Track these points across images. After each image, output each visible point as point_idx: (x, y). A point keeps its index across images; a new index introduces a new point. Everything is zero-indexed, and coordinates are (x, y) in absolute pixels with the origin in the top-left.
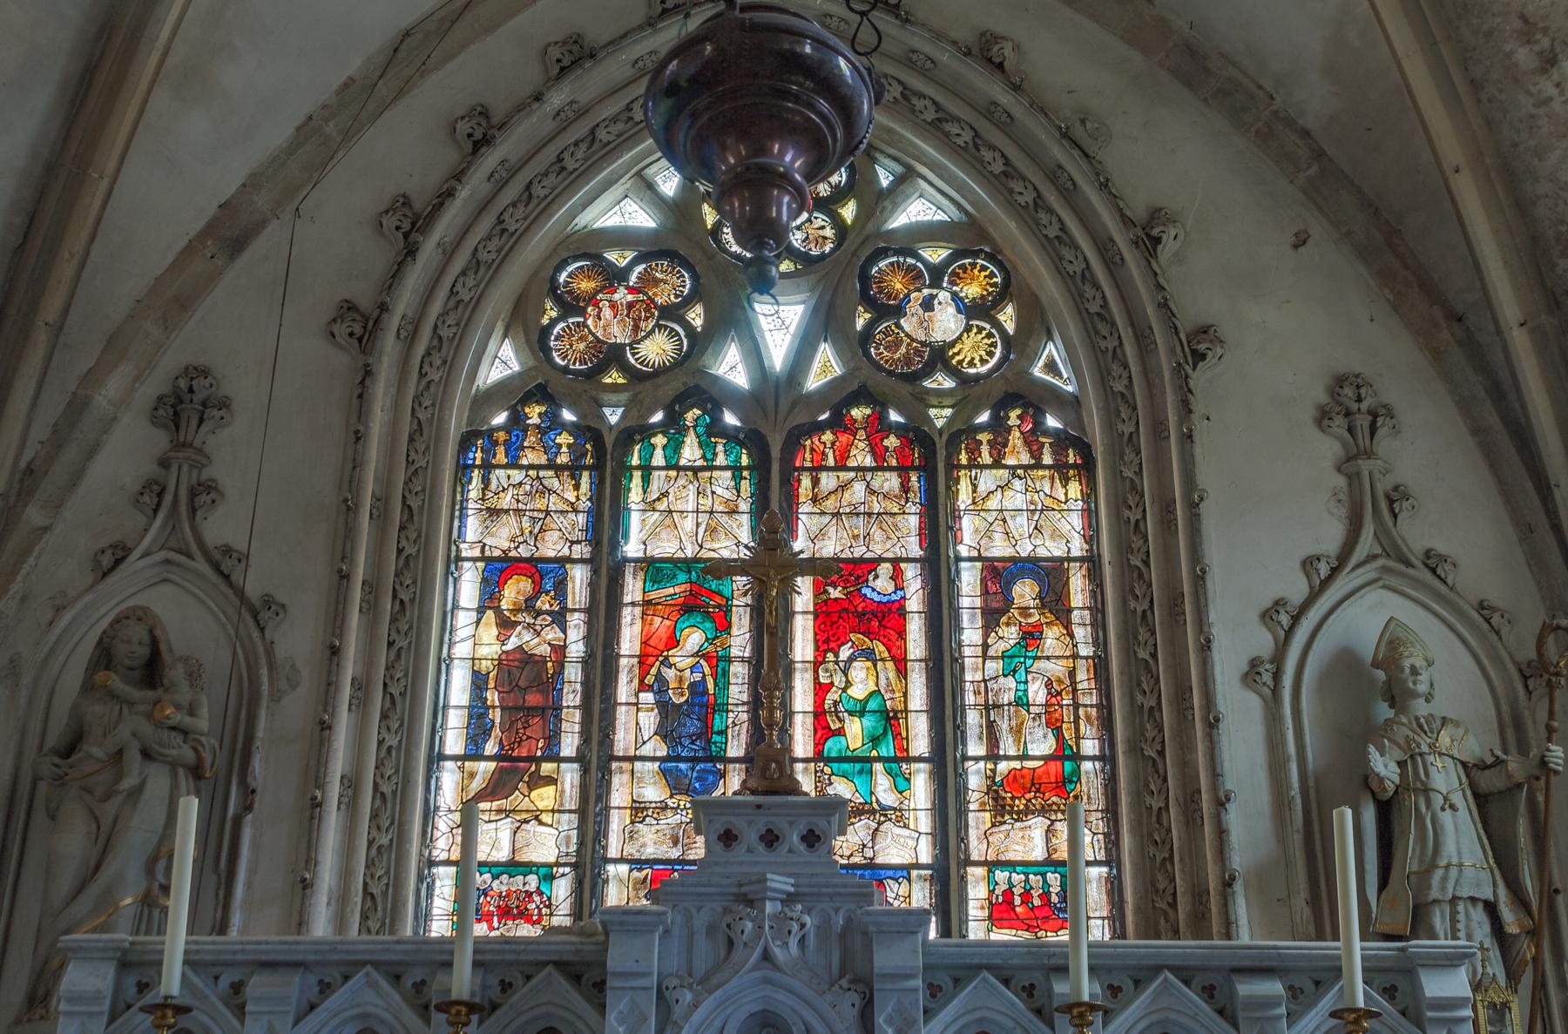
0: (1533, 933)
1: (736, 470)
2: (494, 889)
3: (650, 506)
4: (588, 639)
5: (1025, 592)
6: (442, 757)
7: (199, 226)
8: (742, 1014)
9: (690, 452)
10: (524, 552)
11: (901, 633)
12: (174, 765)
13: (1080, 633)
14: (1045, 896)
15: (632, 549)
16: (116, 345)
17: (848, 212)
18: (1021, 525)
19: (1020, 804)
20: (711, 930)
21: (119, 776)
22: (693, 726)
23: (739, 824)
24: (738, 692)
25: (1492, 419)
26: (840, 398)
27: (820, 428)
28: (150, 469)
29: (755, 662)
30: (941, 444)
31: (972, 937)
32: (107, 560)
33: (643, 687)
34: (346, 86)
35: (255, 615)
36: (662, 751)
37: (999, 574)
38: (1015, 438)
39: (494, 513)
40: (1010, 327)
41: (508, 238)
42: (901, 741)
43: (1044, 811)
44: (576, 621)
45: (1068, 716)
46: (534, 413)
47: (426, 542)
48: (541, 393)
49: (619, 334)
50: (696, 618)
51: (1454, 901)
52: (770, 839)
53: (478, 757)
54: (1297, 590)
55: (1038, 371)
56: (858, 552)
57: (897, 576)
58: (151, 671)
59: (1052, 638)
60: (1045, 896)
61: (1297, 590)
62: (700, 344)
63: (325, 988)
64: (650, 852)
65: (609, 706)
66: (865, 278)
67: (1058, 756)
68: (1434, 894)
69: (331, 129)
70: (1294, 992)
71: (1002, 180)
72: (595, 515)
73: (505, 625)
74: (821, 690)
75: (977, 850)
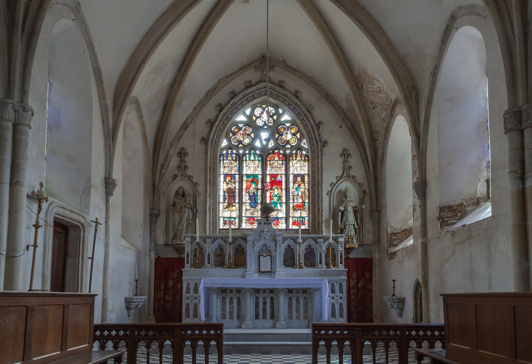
0: (359, 228)
1: (259, 160)
2: (229, 221)
3: (247, 166)
4: (239, 186)
5: (299, 179)
7: (181, 126)
9: (252, 158)
10: (229, 173)
11: (282, 185)
13: (306, 185)
15: (244, 173)
16: (171, 145)
17: (275, 117)
18: (299, 169)
21: (182, 210)
22: (253, 198)
23: (261, 222)
25: (364, 156)
26: (273, 149)
27: (270, 154)
28: (178, 164)
30: (288, 156)
34: (200, 101)
37: (296, 176)
38: (299, 155)
39: (225, 167)
40: (299, 137)
41: (225, 125)
42: (281, 201)
43: (300, 210)
44: (237, 183)
46: (230, 151)
47: (216, 173)
48: (231, 148)
49: (241, 139)
53: (224, 202)
54: (335, 181)
55: (302, 144)
56: (276, 173)
57: (281, 177)
58: (184, 195)
59: (302, 185)
61: (335, 181)
62: (254, 140)
63: (214, 240)
64: (248, 216)
65: (242, 195)
66: (277, 129)
69: (198, 108)
70: (324, 240)
71: (298, 115)
72: (239, 167)
73: (227, 184)
75: (291, 215)
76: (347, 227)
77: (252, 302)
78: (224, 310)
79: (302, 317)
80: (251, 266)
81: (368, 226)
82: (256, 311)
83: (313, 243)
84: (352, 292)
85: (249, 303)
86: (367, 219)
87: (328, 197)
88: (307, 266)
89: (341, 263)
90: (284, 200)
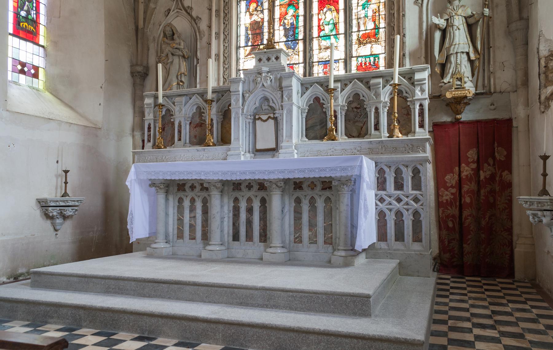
6: (240, 47)
8: (260, 98)
12: (179, 56)
14: (370, 63)
19: (365, 42)
20: (253, 81)
22: (291, 33)
23: (262, 57)
24: (301, 23)
29: (305, 16)
31: (316, 75)
32: (167, 13)
33: (280, 25)
35: (195, 21)
36: (285, 39)
42: (337, 31)
43: (370, 42)
45: (377, 18)
50: (291, 7)
51: (457, 53)
52: (269, 59)
53: (247, 46)
60: (370, 63)
67: (375, 29)
68: (451, 52)
73: (251, 15)
74: (319, 20)
76: (453, 59)
77: (226, 208)
78: (180, 221)
79: (321, 239)
80: (238, 139)
81: (503, 54)
82: (234, 224)
83: (361, 87)
84: (465, 188)
85: (221, 209)
86: (500, 41)
87: (417, 8)
88: (349, 135)
89: (422, 126)
90: (342, 29)
